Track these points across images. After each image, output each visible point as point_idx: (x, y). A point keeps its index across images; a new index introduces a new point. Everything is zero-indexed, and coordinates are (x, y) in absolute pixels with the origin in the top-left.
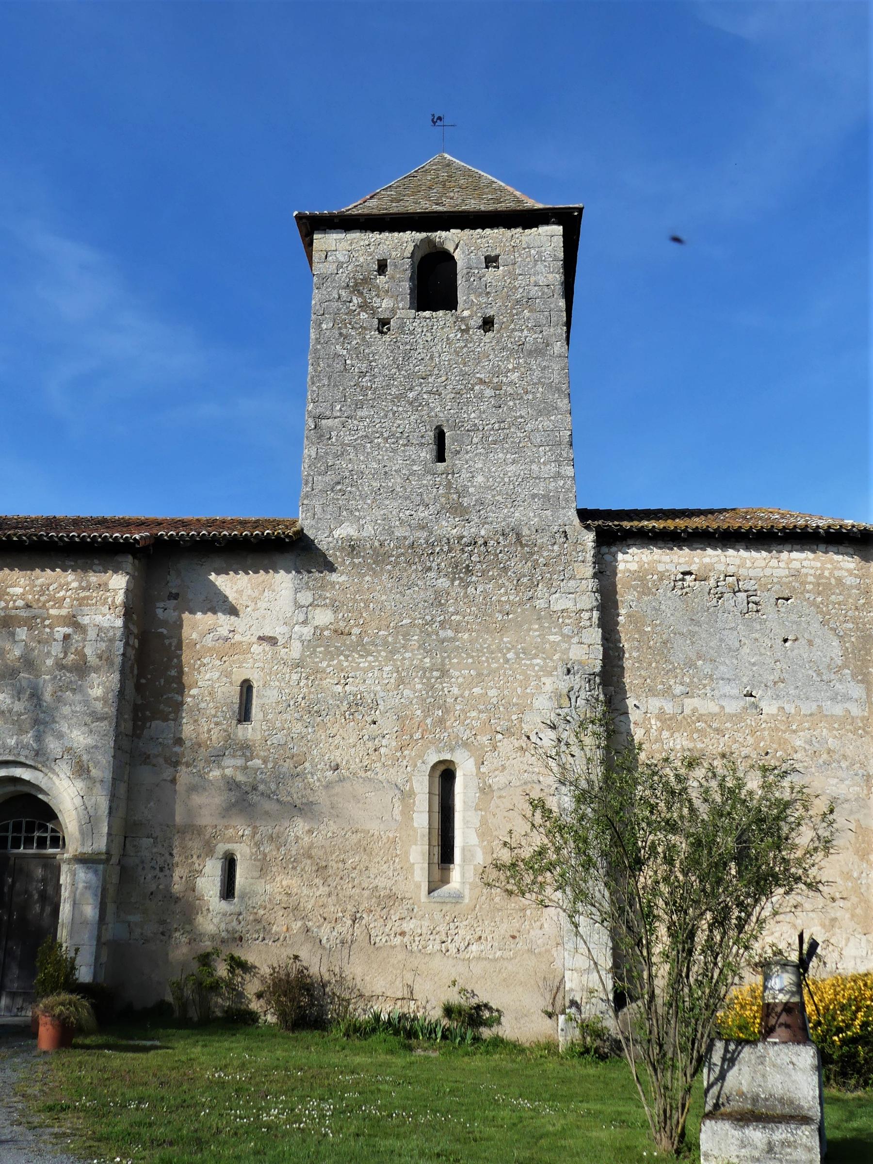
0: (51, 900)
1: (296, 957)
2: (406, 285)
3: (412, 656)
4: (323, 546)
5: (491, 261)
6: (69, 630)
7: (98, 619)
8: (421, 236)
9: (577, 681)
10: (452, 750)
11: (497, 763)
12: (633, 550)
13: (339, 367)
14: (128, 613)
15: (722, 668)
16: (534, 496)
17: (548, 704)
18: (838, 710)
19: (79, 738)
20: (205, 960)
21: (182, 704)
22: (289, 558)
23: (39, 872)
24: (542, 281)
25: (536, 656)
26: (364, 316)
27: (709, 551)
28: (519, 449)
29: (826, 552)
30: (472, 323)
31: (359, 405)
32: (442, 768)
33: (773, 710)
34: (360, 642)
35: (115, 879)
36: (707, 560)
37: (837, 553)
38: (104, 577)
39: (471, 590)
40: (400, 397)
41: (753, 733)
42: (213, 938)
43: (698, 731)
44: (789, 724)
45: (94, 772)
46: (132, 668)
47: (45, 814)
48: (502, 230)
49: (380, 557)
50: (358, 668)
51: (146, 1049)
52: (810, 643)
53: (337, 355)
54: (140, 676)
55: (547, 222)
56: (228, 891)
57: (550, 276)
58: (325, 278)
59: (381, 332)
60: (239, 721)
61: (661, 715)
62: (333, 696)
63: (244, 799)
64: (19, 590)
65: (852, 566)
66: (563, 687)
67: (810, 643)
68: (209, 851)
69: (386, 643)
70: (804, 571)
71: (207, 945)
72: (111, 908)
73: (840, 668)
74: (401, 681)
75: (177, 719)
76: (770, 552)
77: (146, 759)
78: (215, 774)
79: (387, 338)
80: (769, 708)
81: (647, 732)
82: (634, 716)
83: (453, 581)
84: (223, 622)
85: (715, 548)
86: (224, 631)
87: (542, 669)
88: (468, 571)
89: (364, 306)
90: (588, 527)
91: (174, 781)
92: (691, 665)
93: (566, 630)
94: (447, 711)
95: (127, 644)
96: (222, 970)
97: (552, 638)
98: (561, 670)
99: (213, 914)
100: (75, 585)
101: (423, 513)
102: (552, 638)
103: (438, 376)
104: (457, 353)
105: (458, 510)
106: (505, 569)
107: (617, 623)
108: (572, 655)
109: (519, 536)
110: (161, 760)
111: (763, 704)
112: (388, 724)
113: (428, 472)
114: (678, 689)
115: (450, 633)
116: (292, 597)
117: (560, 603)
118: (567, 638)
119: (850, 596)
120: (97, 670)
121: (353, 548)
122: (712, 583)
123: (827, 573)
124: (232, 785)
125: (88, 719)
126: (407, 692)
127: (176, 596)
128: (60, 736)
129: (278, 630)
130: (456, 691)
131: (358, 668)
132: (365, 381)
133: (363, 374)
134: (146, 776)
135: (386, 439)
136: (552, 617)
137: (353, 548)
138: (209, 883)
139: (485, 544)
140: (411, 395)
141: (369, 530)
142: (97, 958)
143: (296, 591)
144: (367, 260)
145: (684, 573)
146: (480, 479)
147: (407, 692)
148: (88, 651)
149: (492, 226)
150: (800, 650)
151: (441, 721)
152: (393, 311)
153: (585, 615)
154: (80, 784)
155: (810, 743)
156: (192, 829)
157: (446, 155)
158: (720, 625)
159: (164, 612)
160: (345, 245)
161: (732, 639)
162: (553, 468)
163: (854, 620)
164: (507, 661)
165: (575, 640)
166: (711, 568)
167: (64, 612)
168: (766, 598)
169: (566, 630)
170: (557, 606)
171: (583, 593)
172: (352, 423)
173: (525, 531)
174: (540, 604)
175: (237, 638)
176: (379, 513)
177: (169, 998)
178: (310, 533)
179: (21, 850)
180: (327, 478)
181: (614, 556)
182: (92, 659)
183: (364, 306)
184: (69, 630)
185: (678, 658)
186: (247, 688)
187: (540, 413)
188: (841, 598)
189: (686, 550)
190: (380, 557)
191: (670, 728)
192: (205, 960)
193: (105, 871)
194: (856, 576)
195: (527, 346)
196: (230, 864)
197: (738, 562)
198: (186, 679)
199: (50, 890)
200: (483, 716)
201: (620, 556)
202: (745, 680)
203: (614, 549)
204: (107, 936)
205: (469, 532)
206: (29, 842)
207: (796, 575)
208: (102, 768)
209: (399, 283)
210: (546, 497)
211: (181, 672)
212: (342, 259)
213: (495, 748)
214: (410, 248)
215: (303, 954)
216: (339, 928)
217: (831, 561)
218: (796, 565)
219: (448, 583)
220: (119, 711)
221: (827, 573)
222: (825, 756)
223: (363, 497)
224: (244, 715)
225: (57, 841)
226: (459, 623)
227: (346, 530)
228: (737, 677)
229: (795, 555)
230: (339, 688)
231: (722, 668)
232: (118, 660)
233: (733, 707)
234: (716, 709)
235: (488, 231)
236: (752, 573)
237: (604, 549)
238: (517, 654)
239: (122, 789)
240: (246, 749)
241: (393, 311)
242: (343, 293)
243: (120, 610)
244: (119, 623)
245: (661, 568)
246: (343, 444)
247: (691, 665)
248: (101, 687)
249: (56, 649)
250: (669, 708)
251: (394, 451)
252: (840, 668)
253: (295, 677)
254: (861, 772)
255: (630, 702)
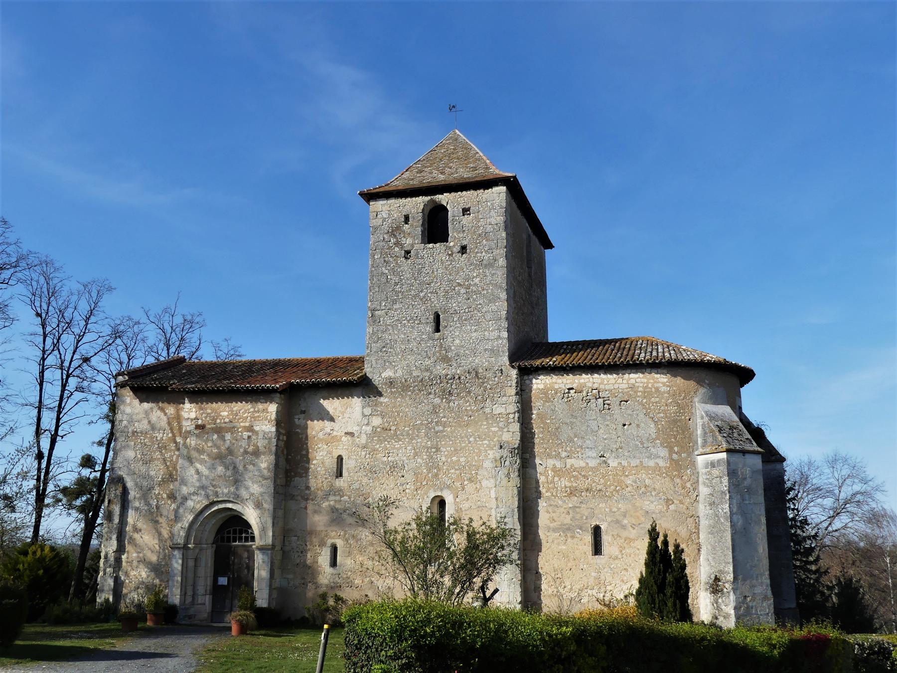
0: (250, 569)
1: (366, 596)
2: (419, 229)
3: (422, 441)
4: (376, 383)
5: (466, 211)
6: (250, 434)
7: (264, 427)
8: (427, 199)
9: (505, 452)
10: (441, 490)
11: (465, 497)
12: (541, 377)
13: (384, 280)
14: (278, 423)
15: (588, 442)
16: (486, 350)
17: (491, 465)
18: (651, 463)
19: (256, 489)
20: (324, 597)
21: (309, 468)
22: (359, 390)
23: (246, 555)
24: (493, 221)
25: (485, 439)
26: (397, 249)
27: (584, 376)
28: (478, 323)
29: (650, 373)
30: (455, 250)
31: (394, 302)
32: (438, 500)
33: (615, 464)
34: (395, 434)
35: (279, 557)
36: (582, 381)
37: (657, 373)
38: (265, 405)
39: (451, 404)
40: (415, 296)
41: (603, 477)
42: (327, 586)
43: (573, 476)
44: (624, 472)
45: (265, 506)
46: (283, 451)
47: (247, 525)
48: (472, 191)
49: (405, 387)
50: (395, 448)
51: (281, 636)
52: (638, 426)
53: (383, 273)
54: (288, 455)
55: (497, 185)
56: (334, 563)
57: (498, 218)
58: (376, 228)
59: (406, 258)
60: (337, 477)
61: (554, 470)
62: (383, 463)
63: (337, 517)
64: (226, 414)
65: (665, 380)
66: (498, 456)
67: (638, 426)
68: (322, 544)
69: (408, 434)
70: (637, 385)
71: (323, 589)
72: (277, 572)
73: (655, 439)
74: (416, 454)
75: (307, 476)
76: (618, 374)
77: (292, 497)
78: (325, 504)
79: (409, 261)
80: (613, 463)
81: (547, 477)
82: (540, 469)
83: (442, 399)
84: (327, 424)
85: (587, 374)
86: (328, 430)
87: (488, 446)
88: (450, 394)
89: (397, 244)
90: (513, 367)
91: (306, 508)
92: (571, 440)
93: (501, 424)
94: (439, 470)
95: (278, 440)
96: (331, 602)
97: (493, 429)
98: (498, 446)
99: (326, 574)
100: (252, 410)
101: (428, 362)
102: (493, 429)
103: (436, 283)
104: (446, 268)
105: (446, 360)
106: (469, 392)
107: (531, 419)
108: (504, 438)
109: (477, 373)
110: (299, 498)
111: (609, 461)
112: (410, 477)
113: (430, 338)
114: (564, 454)
115: (441, 428)
116: (361, 411)
117: (498, 409)
118: (501, 429)
119: (663, 398)
120: (264, 454)
121: (391, 383)
122: (584, 394)
123: (650, 385)
124: (333, 510)
125: (260, 479)
126: (419, 460)
127: (304, 412)
128: (247, 488)
129: (354, 429)
130: (444, 459)
131: (395, 448)
132: (398, 288)
133: (396, 284)
134: (292, 505)
135: (408, 321)
136: (494, 417)
137: (391, 383)
138: (324, 559)
139: (459, 378)
140: (422, 295)
141: (400, 373)
142: (270, 595)
143: (363, 408)
144: (398, 216)
145: (569, 389)
146: (457, 341)
147: (419, 460)
148: (259, 444)
149: (466, 190)
150: (631, 430)
151: (436, 475)
152: (412, 246)
153: (511, 416)
154: (258, 511)
155: (635, 482)
156: (311, 533)
157: (457, 131)
158: (587, 418)
159: (298, 420)
160: (386, 208)
161: (594, 425)
162: (496, 333)
163: (664, 412)
164: (470, 442)
165: (505, 430)
166: (584, 385)
167: (247, 424)
168: (614, 401)
169: (501, 424)
170: (496, 412)
171: (510, 404)
172: (391, 313)
173: (480, 371)
174: (488, 410)
175: (335, 433)
176: (404, 363)
177: (307, 615)
178: (369, 375)
179: (237, 543)
180: (378, 345)
181: (531, 381)
182: (261, 449)
183: (397, 244)
184: (250, 434)
185: (564, 437)
186: (340, 459)
187: (490, 301)
188: (657, 399)
189: (571, 375)
190: (405, 387)
191: (559, 476)
192: (324, 597)
193: (272, 554)
194: (668, 386)
195: (485, 262)
196: (334, 549)
197: (599, 381)
198: (310, 456)
199: (251, 564)
200: (458, 472)
201: (534, 381)
202: (600, 448)
203: (531, 377)
204: (277, 584)
205: (451, 371)
206: (240, 539)
207: (632, 387)
208: (268, 505)
209: (416, 228)
210: (492, 350)
211: (308, 452)
212: (385, 216)
213: (463, 489)
214: (422, 207)
215: (370, 594)
216: (387, 581)
217: (653, 378)
218: (633, 381)
219: (439, 401)
220: (276, 475)
221: (650, 385)
222: (643, 489)
223: (397, 355)
224: (339, 474)
225: (253, 539)
226: (445, 422)
227: (388, 373)
228: (596, 447)
229: (632, 375)
230: (385, 459)
231: (588, 442)
232: (274, 449)
233: (593, 463)
234: (584, 465)
235: (464, 193)
236: (607, 387)
237: (526, 377)
238: (475, 438)
239: (280, 513)
240: (339, 492)
241: (412, 246)
242: (386, 236)
243: (274, 423)
244: (274, 429)
245: (556, 386)
246: (386, 325)
247: (571, 440)
248: (265, 463)
249: (244, 444)
250: (558, 464)
251: (413, 327)
252: (655, 439)
253: (363, 453)
254: (663, 497)
255: (538, 461)
